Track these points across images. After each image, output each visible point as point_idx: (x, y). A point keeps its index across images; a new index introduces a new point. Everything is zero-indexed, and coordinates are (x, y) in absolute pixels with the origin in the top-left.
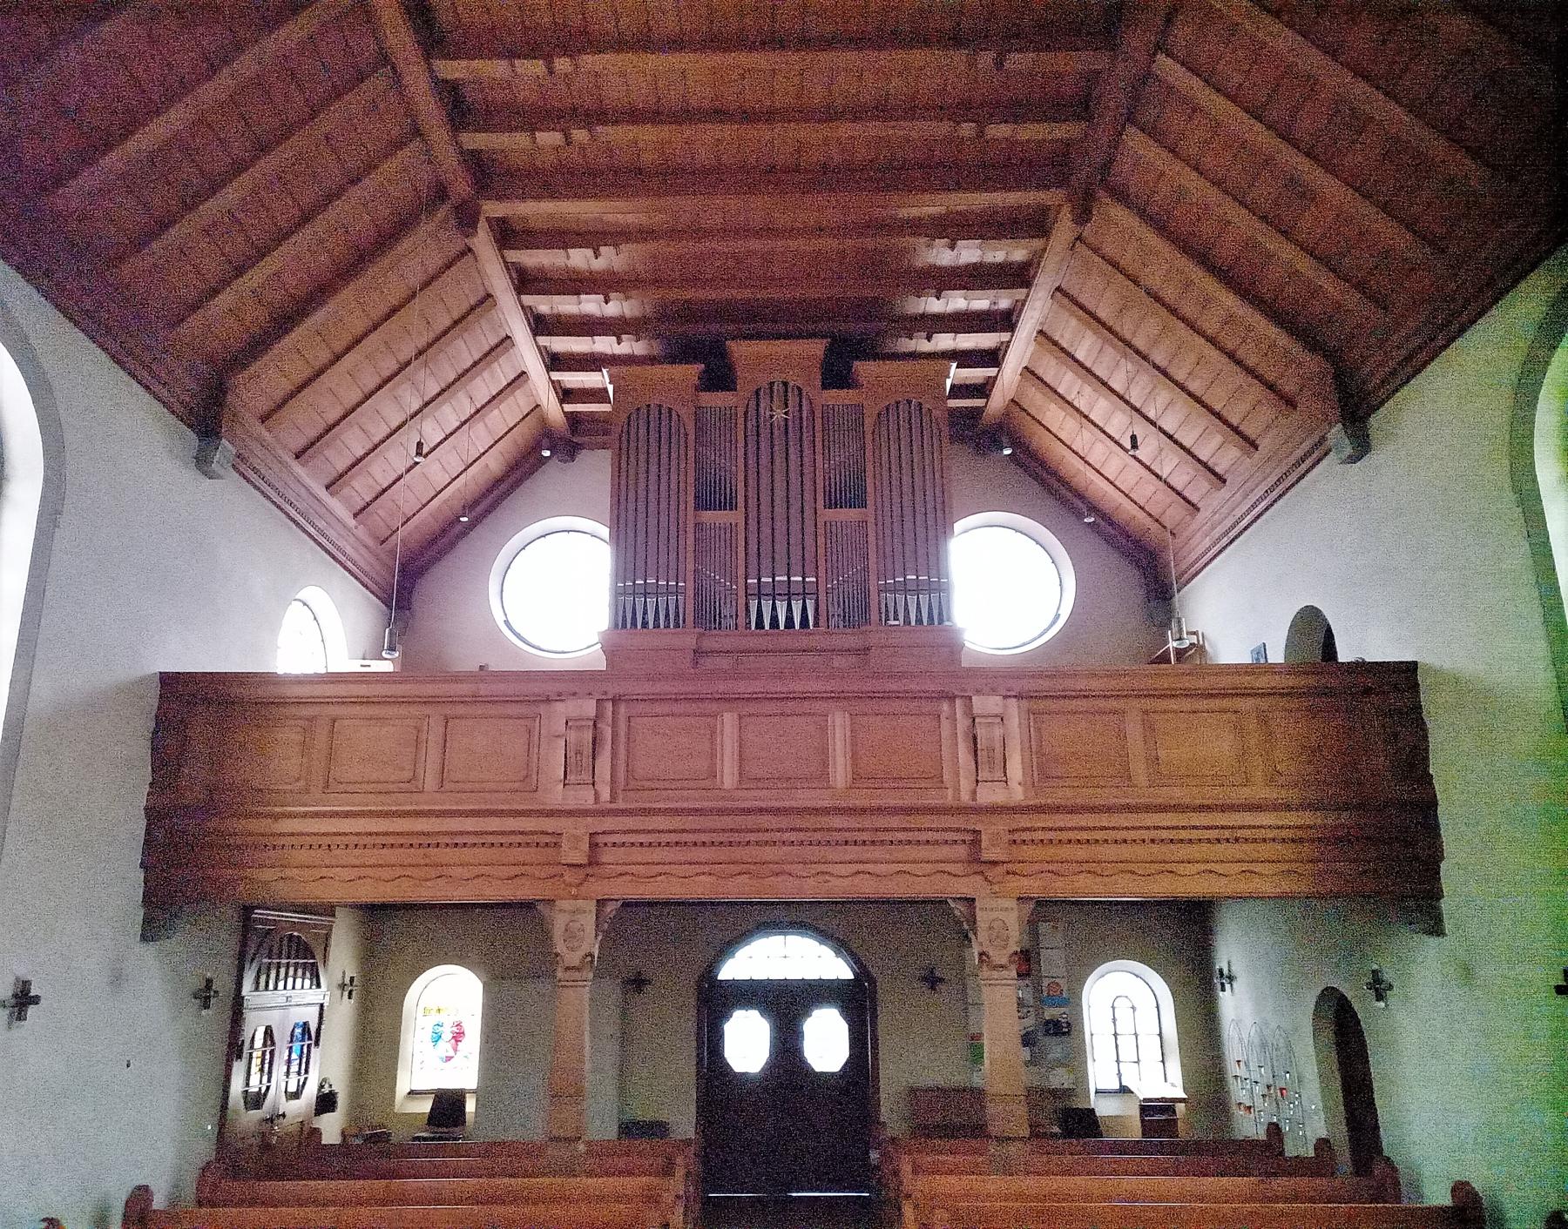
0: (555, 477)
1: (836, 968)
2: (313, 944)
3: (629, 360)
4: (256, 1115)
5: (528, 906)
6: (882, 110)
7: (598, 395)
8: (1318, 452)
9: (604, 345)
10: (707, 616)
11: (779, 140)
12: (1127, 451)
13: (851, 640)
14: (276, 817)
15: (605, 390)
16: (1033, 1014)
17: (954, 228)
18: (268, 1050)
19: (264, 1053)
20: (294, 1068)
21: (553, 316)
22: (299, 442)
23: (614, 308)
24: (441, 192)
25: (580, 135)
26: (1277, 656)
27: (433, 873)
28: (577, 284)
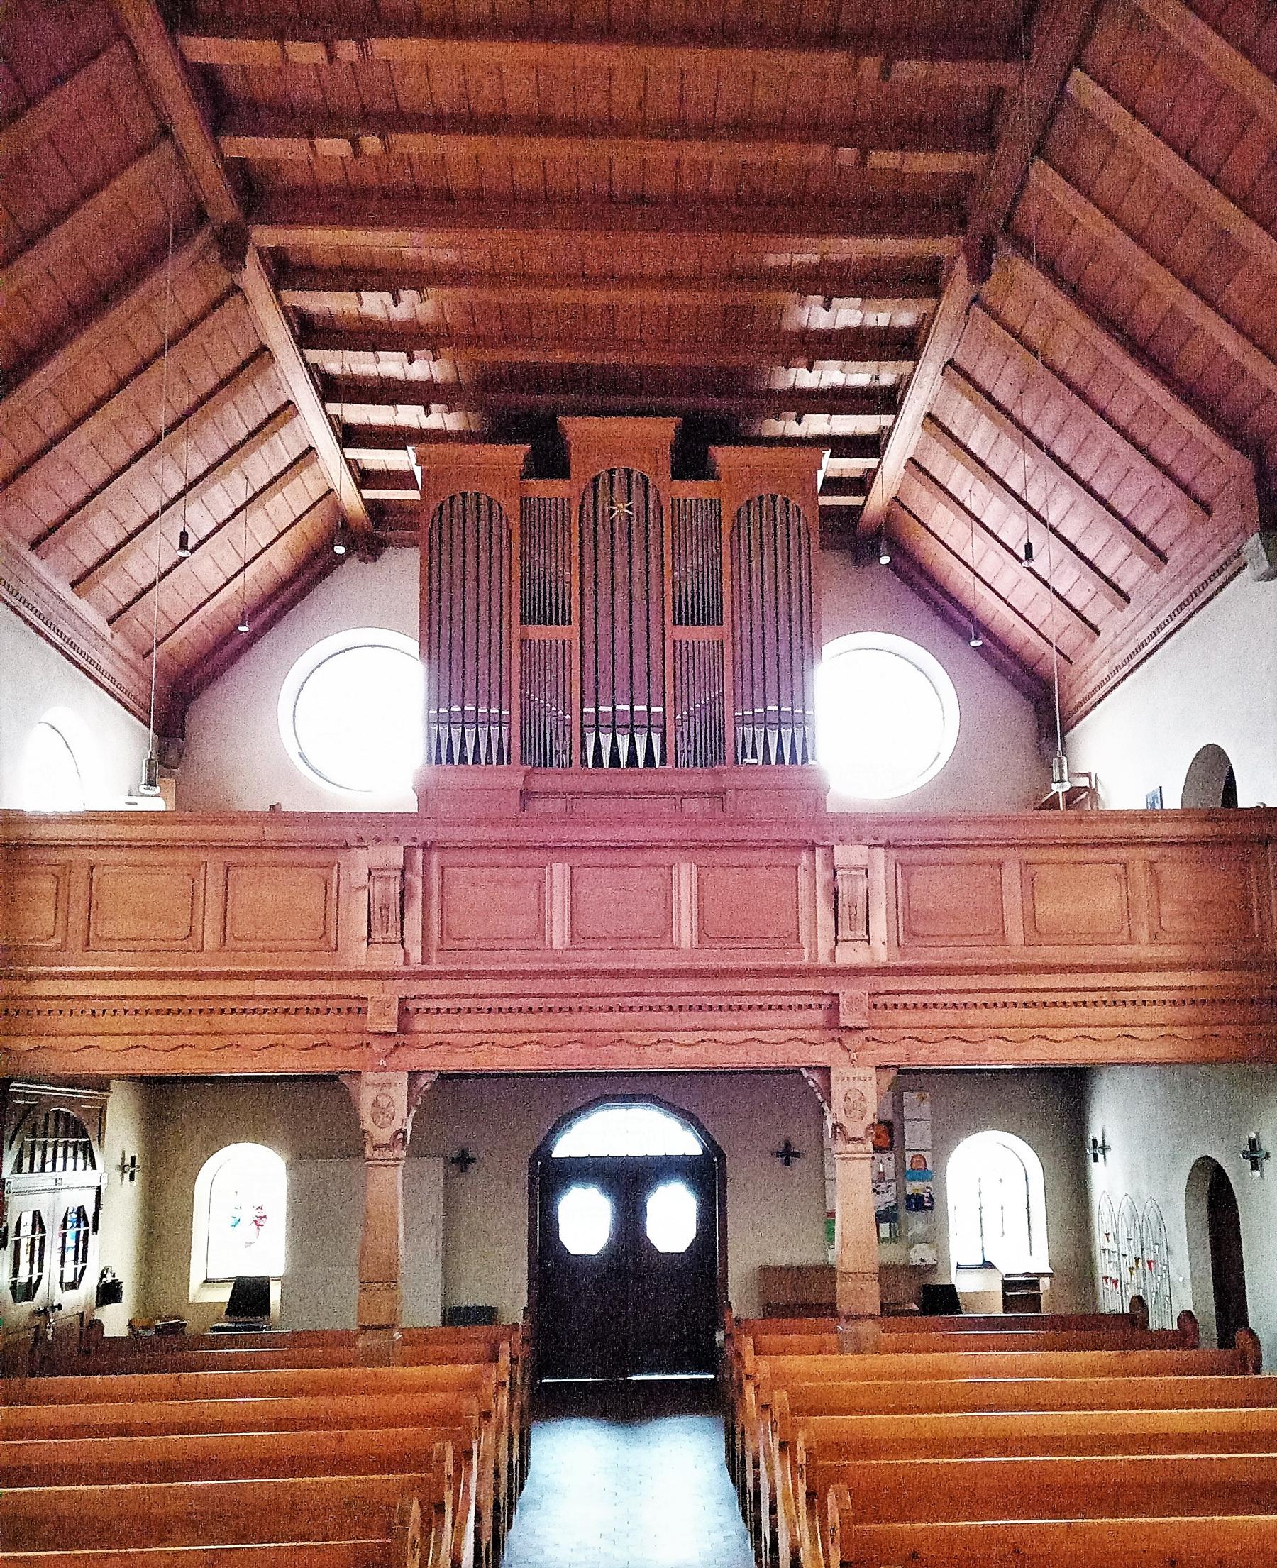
0: (354, 582)
1: (681, 1141)
2: (84, 1119)
3: (440, 436)
4: (26, 1307)
5: (331, 1079)
6: (745, 127)
7: (402, 479)
8: (1232, 567)
9: (409, 416)
10: (537, 753)
11: (620, 161)
12: (1021, 561)
13: (702, 780)
14: (30, 978)
15: (412, 473)
16: (893, 1189)
17: (829, 282)
18: (38, 1236)
19: (33, 1240)
20: (70, 1255)
21: (345, 377)
22: (32, 530)
23: (420, 369)
24: (198, 215)
25: (371, 144)
26: (1173, 801)
27: (218, 1042)
28: (373, 337)
